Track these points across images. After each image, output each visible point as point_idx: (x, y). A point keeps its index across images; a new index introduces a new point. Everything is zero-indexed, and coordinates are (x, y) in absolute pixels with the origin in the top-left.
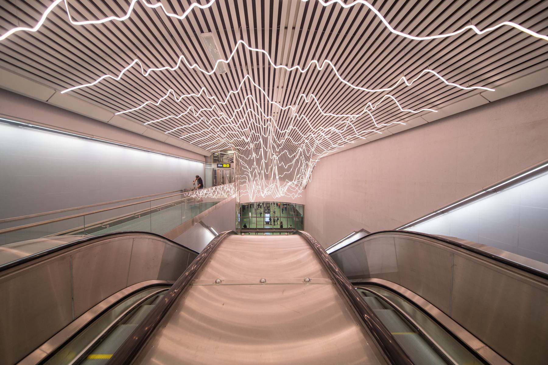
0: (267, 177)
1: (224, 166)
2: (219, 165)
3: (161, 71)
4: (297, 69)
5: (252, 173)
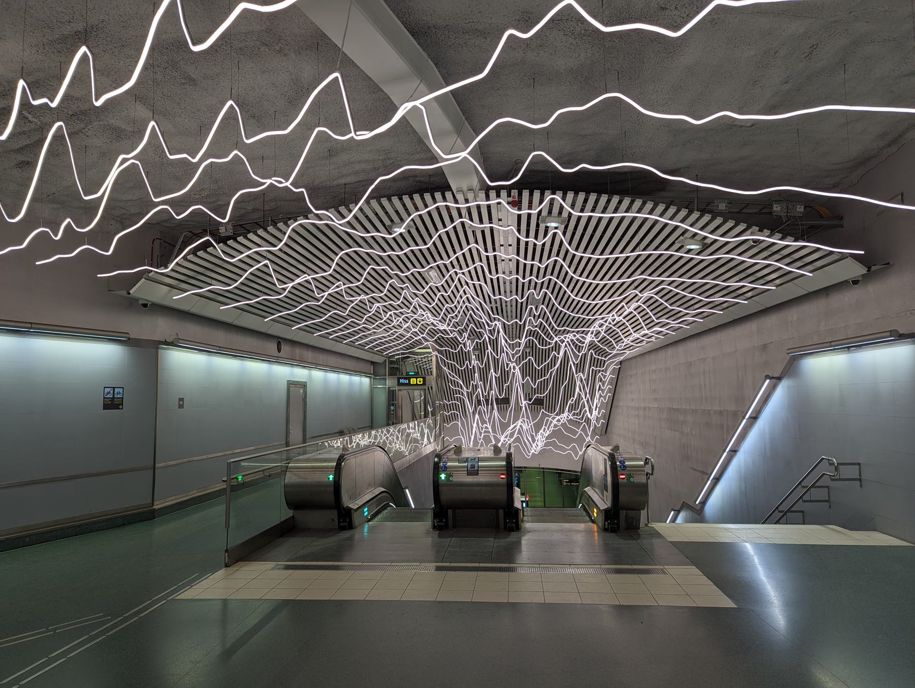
0: (504, 402)
1: (413, 381)
2: (401, 381)
3: (398, 256)
4: (524, 278)
5: (470, 396)
